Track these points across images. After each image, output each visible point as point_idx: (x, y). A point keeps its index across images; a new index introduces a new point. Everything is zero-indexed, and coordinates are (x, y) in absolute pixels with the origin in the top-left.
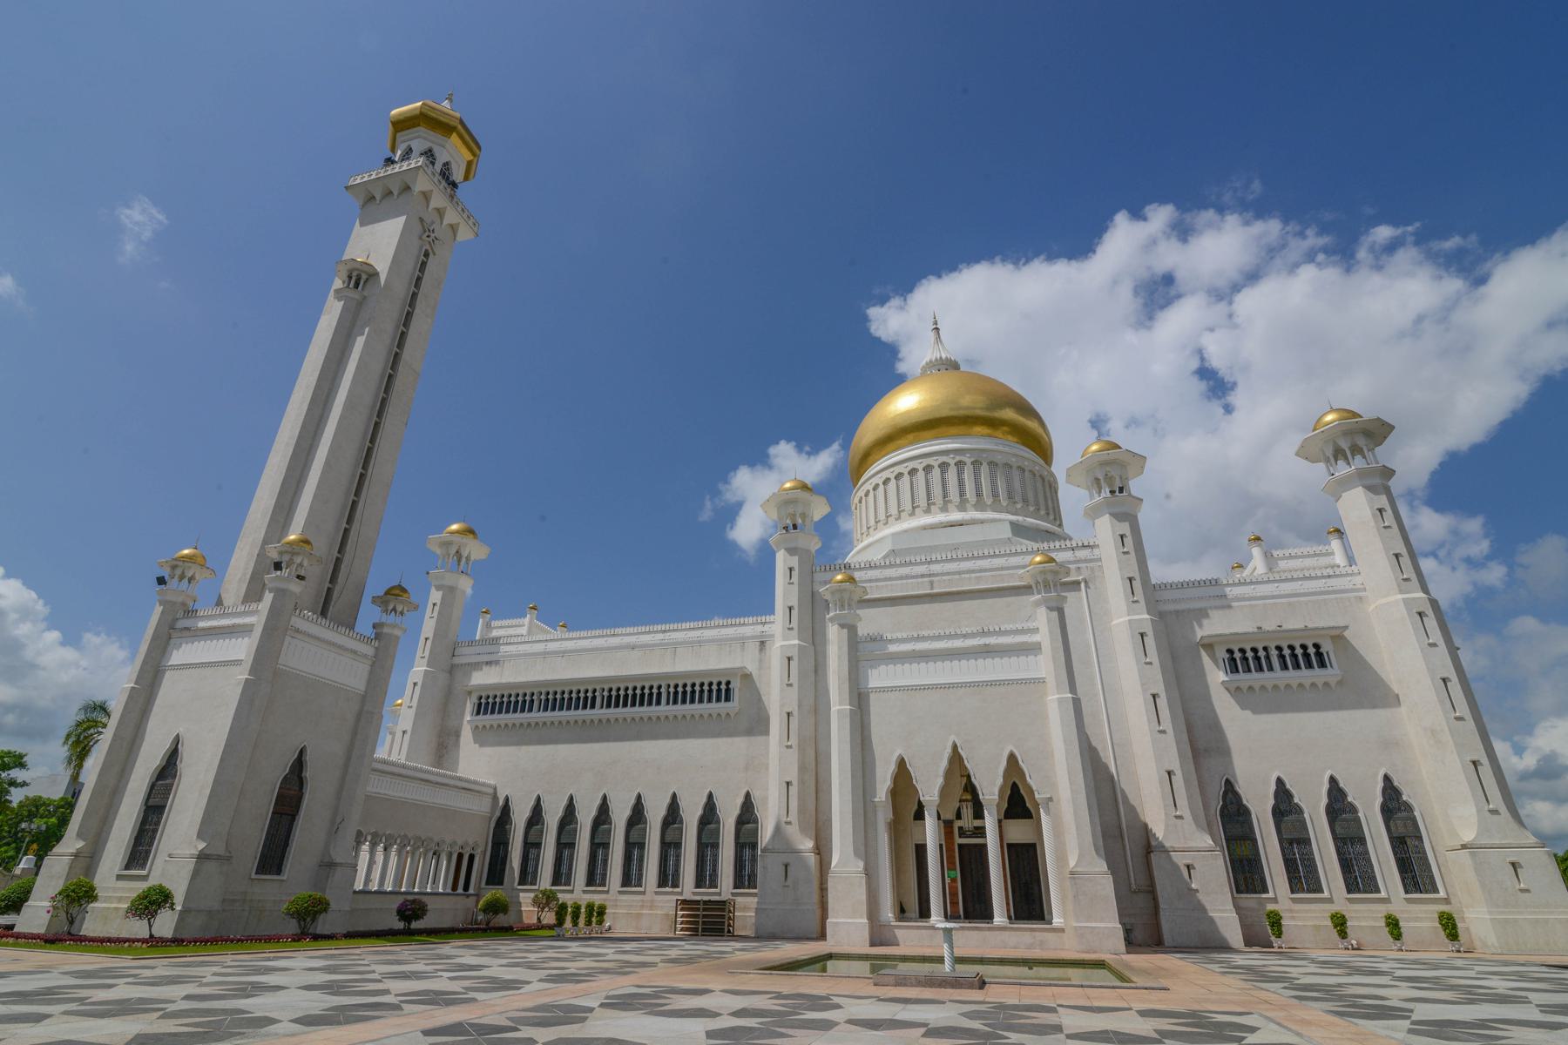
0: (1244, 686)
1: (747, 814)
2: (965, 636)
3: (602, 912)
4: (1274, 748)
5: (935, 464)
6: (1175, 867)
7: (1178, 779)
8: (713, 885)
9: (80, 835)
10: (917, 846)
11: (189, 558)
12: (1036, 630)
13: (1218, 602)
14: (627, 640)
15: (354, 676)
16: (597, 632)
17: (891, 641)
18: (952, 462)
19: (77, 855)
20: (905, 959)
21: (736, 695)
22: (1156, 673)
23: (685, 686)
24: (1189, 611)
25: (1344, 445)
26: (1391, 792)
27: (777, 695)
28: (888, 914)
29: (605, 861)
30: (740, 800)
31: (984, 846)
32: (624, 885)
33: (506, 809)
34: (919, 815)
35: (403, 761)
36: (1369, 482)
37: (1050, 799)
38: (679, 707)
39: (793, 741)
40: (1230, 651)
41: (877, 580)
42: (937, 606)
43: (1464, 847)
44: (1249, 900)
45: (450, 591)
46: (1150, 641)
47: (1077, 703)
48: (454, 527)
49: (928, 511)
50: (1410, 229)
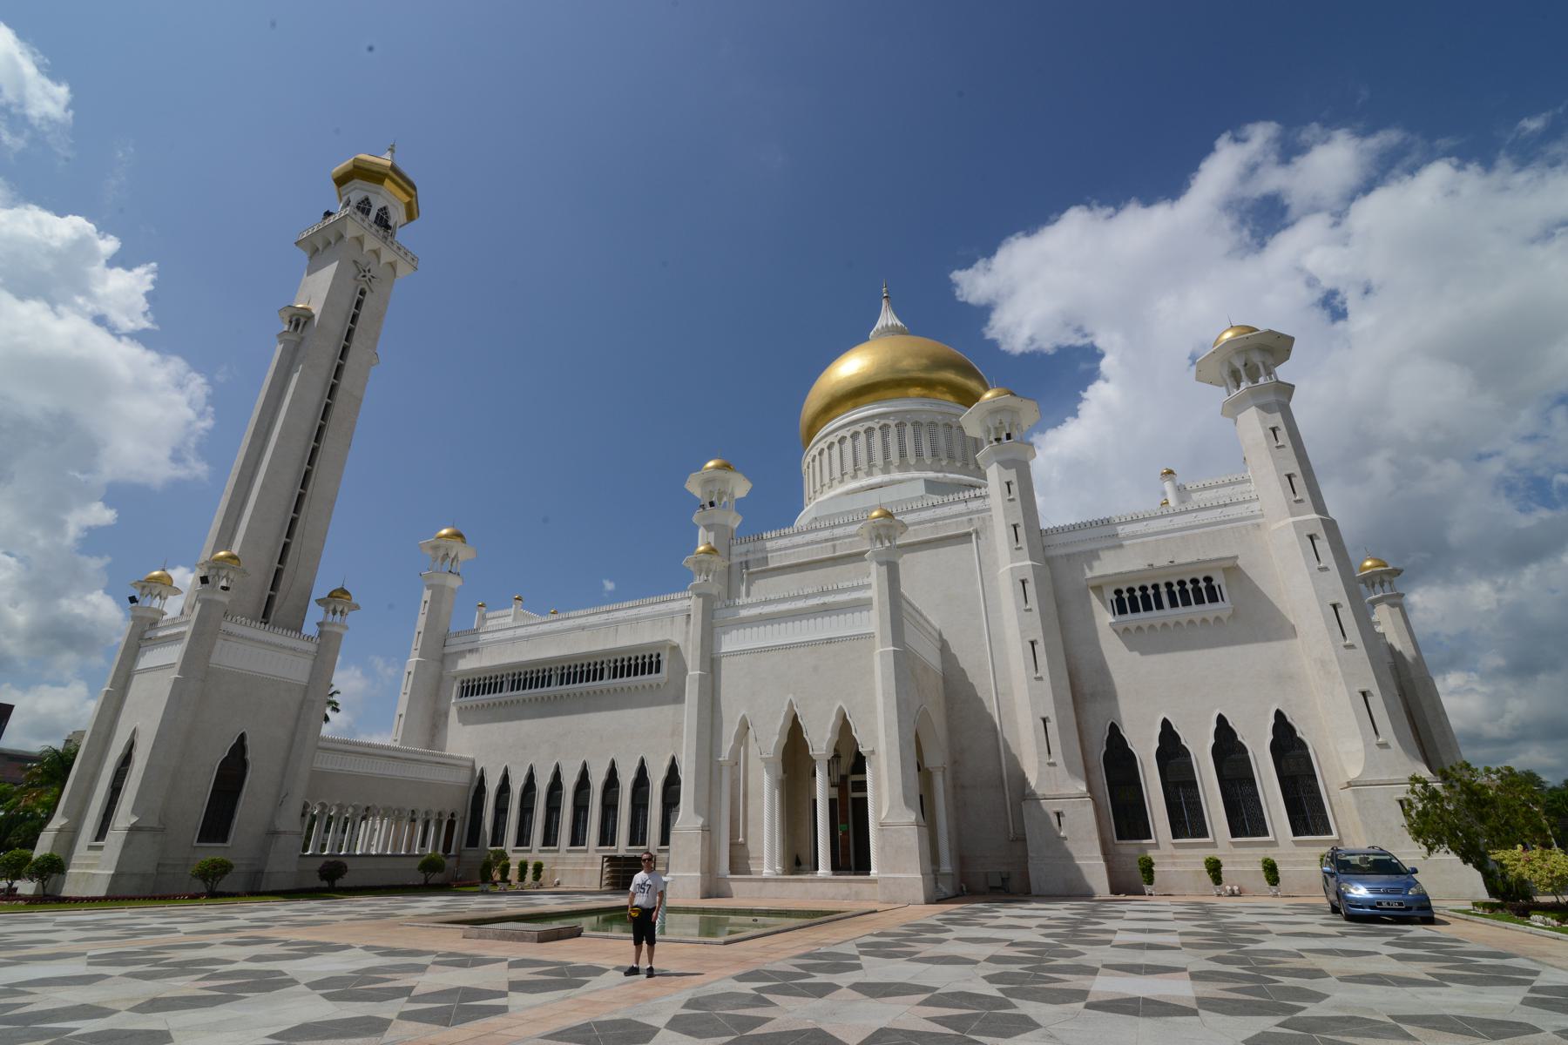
0: (1132, 626)
2: (807, 597)
3: (538, 868)
4: (1168, 691)
5: (861, 430)
6: (1046, 816)
9: (64, 814)
11: (156, 579)
13: (1110, 542)
15: (296, 670)
18: (877, 427)
19: (60, 830)
20: (735, 912)
21: (664, 667)
24: (1080, 553)
25: (1239, 364)
31: (865, 799)
32: (572, 844)
33: (482, 779)
35: (397, 745)
36: (1262, 401)
38: (618, 680)
40: (1118, 592)
42: (839, 569)
44: (1130, 847)
45: (438, 591)
49: (855, 477)
50: (1561, 110)
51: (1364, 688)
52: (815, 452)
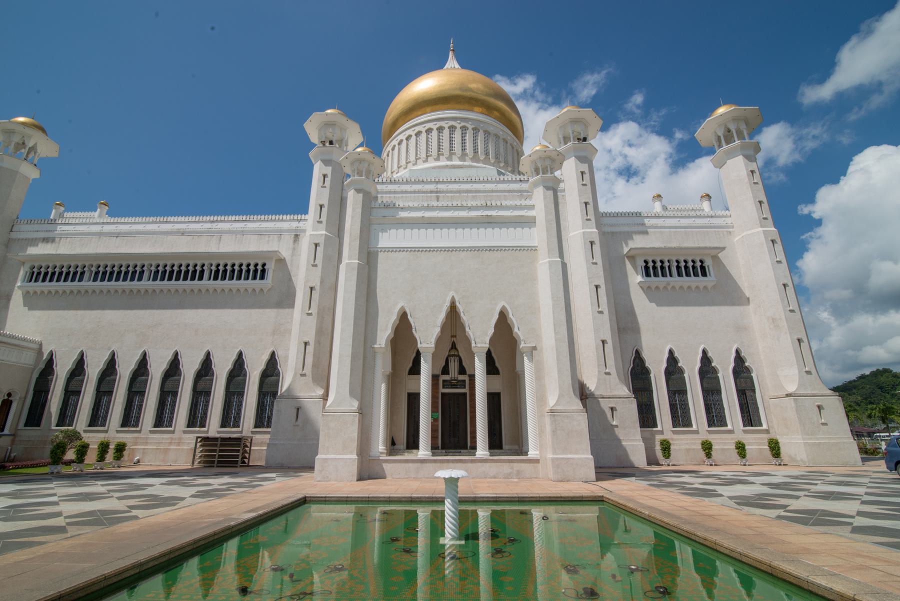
1: (271, 370)
2: (470, 208)
3: (120, 449)
4: (673, 331)
5: (446, 126)
7: (609, 347)
8: (237, 425)
10: (409, 395)
12: (532, 207)
14: (178, 227)
16: (151, 219)
17: (403, 209)
18: (459, 126)
21: (270, 275)
22: (599, 270)
23: (256, 265)
24: (620, 233)
25: (733, 128)
26: (739, 360)
27: (303, 274)
28: (380, 446)
29: (140, 407)
30: (266, 357)
33: (50, 362)
34: (415, 370)
37: (535, 348)
38: (219, 282)
39: (314, 310)
40: (646, 262)
41: (395, 192)
43: (788, 395)
46: (597, 248)
47: (564, 266)
48: (21, 119)
51: (799, 337)
52: (395, 142)
